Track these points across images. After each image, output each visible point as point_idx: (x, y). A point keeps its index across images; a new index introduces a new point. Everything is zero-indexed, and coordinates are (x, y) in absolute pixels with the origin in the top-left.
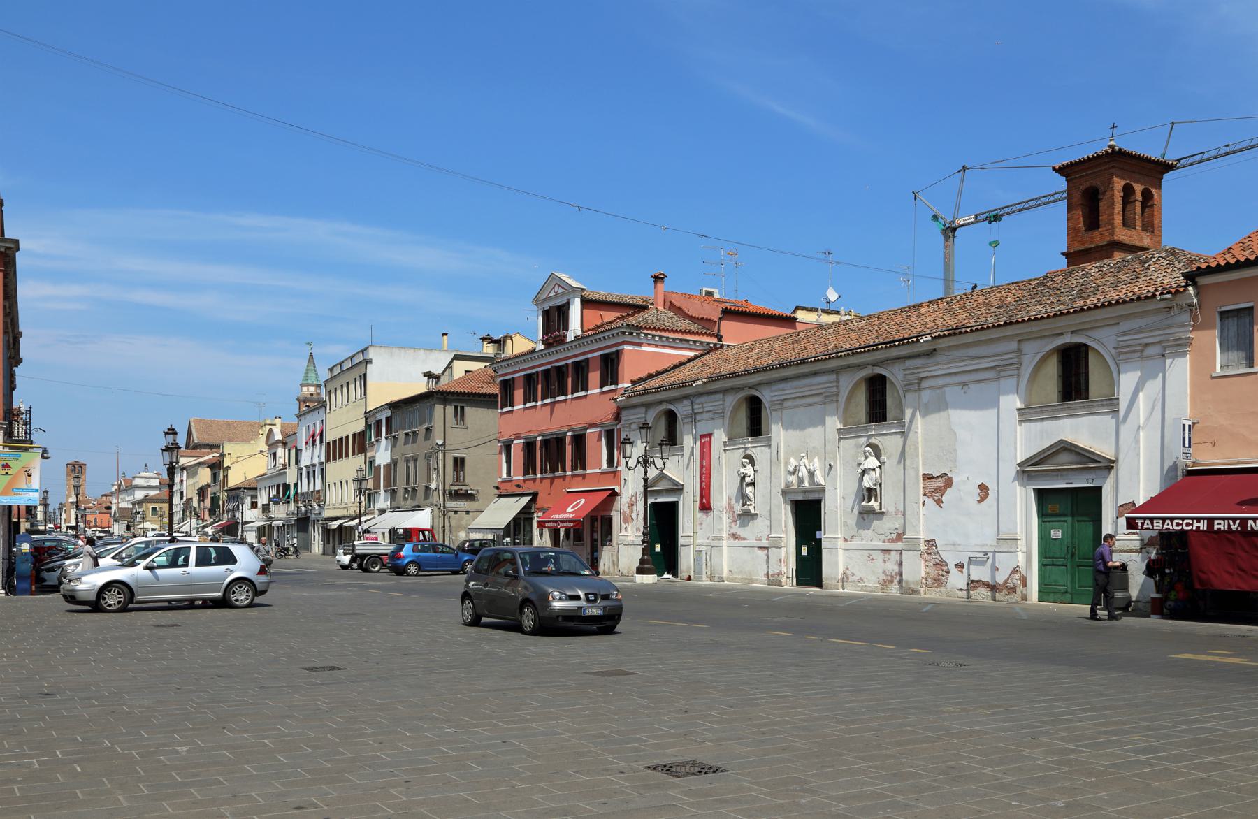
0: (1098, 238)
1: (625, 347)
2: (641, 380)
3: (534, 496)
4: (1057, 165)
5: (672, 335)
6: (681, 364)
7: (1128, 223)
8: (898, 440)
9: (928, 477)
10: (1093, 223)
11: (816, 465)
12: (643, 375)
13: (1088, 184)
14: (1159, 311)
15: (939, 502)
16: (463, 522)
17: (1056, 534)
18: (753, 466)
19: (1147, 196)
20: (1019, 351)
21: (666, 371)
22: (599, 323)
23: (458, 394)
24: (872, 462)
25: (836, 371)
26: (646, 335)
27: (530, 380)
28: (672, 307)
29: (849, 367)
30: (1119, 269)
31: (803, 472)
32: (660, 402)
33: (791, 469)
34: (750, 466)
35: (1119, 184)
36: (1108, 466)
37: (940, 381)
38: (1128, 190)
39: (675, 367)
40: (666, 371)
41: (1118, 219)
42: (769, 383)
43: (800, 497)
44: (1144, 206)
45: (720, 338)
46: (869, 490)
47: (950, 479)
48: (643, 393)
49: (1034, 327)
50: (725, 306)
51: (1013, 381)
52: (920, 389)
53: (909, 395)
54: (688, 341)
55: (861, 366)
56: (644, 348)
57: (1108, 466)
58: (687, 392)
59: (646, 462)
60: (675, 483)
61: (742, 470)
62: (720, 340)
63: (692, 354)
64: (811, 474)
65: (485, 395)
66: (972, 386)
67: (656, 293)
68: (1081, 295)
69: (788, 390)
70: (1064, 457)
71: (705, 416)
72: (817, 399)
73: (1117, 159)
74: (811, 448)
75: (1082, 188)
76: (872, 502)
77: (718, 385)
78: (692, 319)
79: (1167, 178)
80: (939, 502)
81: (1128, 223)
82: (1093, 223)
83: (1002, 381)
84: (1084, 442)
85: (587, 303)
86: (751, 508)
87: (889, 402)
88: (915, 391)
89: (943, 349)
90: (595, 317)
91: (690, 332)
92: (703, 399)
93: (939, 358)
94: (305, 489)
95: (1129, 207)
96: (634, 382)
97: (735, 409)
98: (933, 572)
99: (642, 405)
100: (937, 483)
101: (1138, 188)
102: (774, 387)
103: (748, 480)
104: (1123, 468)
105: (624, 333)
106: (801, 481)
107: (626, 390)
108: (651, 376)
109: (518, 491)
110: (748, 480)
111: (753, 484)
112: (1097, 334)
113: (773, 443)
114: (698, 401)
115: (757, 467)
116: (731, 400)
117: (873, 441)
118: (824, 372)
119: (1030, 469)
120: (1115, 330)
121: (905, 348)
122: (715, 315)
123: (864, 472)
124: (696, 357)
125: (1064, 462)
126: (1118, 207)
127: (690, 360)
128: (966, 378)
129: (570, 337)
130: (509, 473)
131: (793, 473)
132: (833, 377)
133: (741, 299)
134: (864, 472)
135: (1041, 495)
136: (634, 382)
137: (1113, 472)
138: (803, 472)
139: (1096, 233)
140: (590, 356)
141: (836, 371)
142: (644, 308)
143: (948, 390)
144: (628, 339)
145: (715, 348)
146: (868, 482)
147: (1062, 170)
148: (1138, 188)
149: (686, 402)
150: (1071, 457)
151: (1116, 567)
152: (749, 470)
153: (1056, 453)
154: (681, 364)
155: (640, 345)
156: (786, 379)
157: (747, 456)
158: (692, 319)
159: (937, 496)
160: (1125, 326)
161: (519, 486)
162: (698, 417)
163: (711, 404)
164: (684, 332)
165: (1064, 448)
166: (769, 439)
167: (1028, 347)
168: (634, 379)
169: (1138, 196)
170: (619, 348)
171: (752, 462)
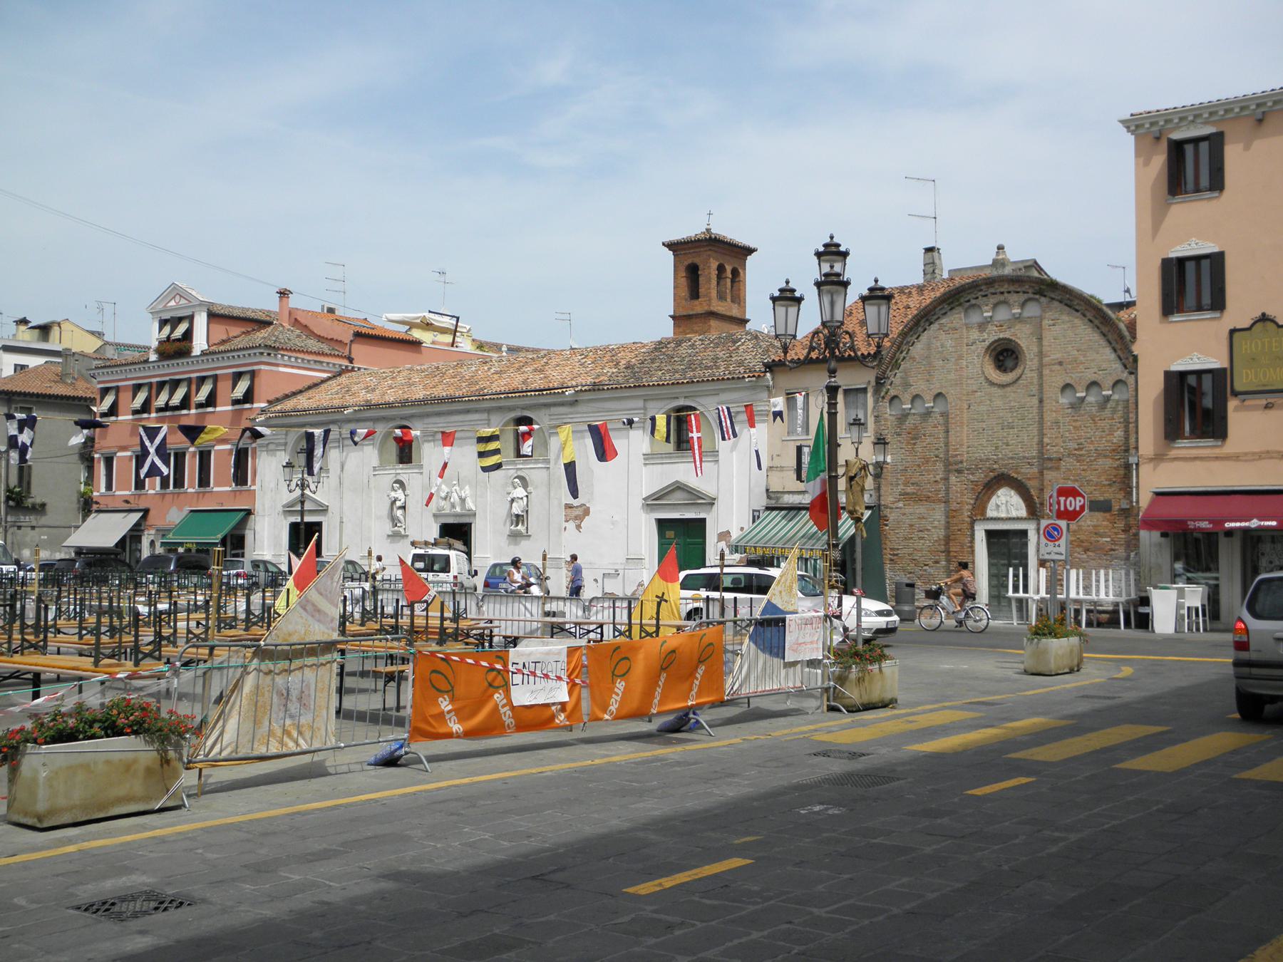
0: (699, 307)
1: (263, 367)
2: (278, 400)
3: (146, 512)
4: (668, 239)
5: (307, 357)
6: (316, 385)
7: (721, 297)
8: (544, 473)
10: (694, 293)
11: (466, 492)
12: (279, 395)
13: (690, 261)
14: (747, 388)
15: (578, 527)
16: (28, 539)
18: (404, 490)
19: (735, 273)
21: (301, 392)
22: (225, 337)
23: (25, 394)
24: (520, 492)
27: (1217, 586)
28: (296, 323)
29: (500, 408)
30: (717, 345)
31: (455, 498)
32: (303, 425)
33: (443, 495)
34: (400, 491)
35: (714, 265)
36: (711, 503)
38: (721, 269)
39: (310, 388)
40: (301, 392)
41: (714, 293)
43: (451, 521)
44: (733, 282)
45: (351, 360)
46: (517, 516)
48: (285, 414)
49: (657, 391)
50: (357, 329)
54: (321, 362)
55: (511, 409)
56: (282, 369)
57: (711, 503)
58: (331, 417)
59: (303, 485)
60: (320, 504)
61: (393, 494)
62: (351, 360)
63: (325, 375)
64: (463, 500)
65: (56, 397)
67: (281, 307)
68: (690, 367)
73: (712, 243)
74: (449, 473)
75: (686, 263)
76: (520, 527)
77: (372, 412)
78: (320, 338)
79: (750, 260)
80: (578, 527)
81: (721, 297)
82: (694, 293)
84: (693, 482)
85: (213, 316)
86: (402, 530)
90: (221, 331)
91: (323, 354)
93: (579, 408)
95: (722, 282)
96: (270, 402)
100: (578, 512)
101: (729, 269)
102: (426, 421)
103: (398, 504)
104: (720, 505)
105: (262, 354)
106: (453, 506)
107: (263, 411)
108: (287, 397)
109: (127, 506)
110: (398, 504)
111: (404, 508)
112: (703, 400)
113: (425, 470)
115: (407, 492)
116: (1226, 364)
117: (520, 473)
118: (476, 411)
119: (655, 500)
122: (347, 337)
123: (513, 500)
124: (329, 379)
125: (678, 498)
126: (714, 282)
127: (324, 381)
129: (196, 351)
130: (109, 486)
131: (445, 499)
134: (513, 500)
135: (661, 523)
136: (270, 402)
137: (715, 507)
138: (455, 498)
139: (696, 302)
142: (270, 323)
144: (265, 359)
145: (347, 370)
146: (517, 509)
147: (671, 246)
148: (729, 269)
150: (684, 495)
151: (1131, 352)
152: (399, 494)
154: (316, 385)
155: (277, 365)
156: (439, 414)
157: (397, 482)
158: (320, 338)
161: (127, 502)
164: (318, 354)
165: (678, 487)
166: (421, 467)
168: (271, 398)
169: (729, 274)
170: (255, 368)
171: (402, 484)
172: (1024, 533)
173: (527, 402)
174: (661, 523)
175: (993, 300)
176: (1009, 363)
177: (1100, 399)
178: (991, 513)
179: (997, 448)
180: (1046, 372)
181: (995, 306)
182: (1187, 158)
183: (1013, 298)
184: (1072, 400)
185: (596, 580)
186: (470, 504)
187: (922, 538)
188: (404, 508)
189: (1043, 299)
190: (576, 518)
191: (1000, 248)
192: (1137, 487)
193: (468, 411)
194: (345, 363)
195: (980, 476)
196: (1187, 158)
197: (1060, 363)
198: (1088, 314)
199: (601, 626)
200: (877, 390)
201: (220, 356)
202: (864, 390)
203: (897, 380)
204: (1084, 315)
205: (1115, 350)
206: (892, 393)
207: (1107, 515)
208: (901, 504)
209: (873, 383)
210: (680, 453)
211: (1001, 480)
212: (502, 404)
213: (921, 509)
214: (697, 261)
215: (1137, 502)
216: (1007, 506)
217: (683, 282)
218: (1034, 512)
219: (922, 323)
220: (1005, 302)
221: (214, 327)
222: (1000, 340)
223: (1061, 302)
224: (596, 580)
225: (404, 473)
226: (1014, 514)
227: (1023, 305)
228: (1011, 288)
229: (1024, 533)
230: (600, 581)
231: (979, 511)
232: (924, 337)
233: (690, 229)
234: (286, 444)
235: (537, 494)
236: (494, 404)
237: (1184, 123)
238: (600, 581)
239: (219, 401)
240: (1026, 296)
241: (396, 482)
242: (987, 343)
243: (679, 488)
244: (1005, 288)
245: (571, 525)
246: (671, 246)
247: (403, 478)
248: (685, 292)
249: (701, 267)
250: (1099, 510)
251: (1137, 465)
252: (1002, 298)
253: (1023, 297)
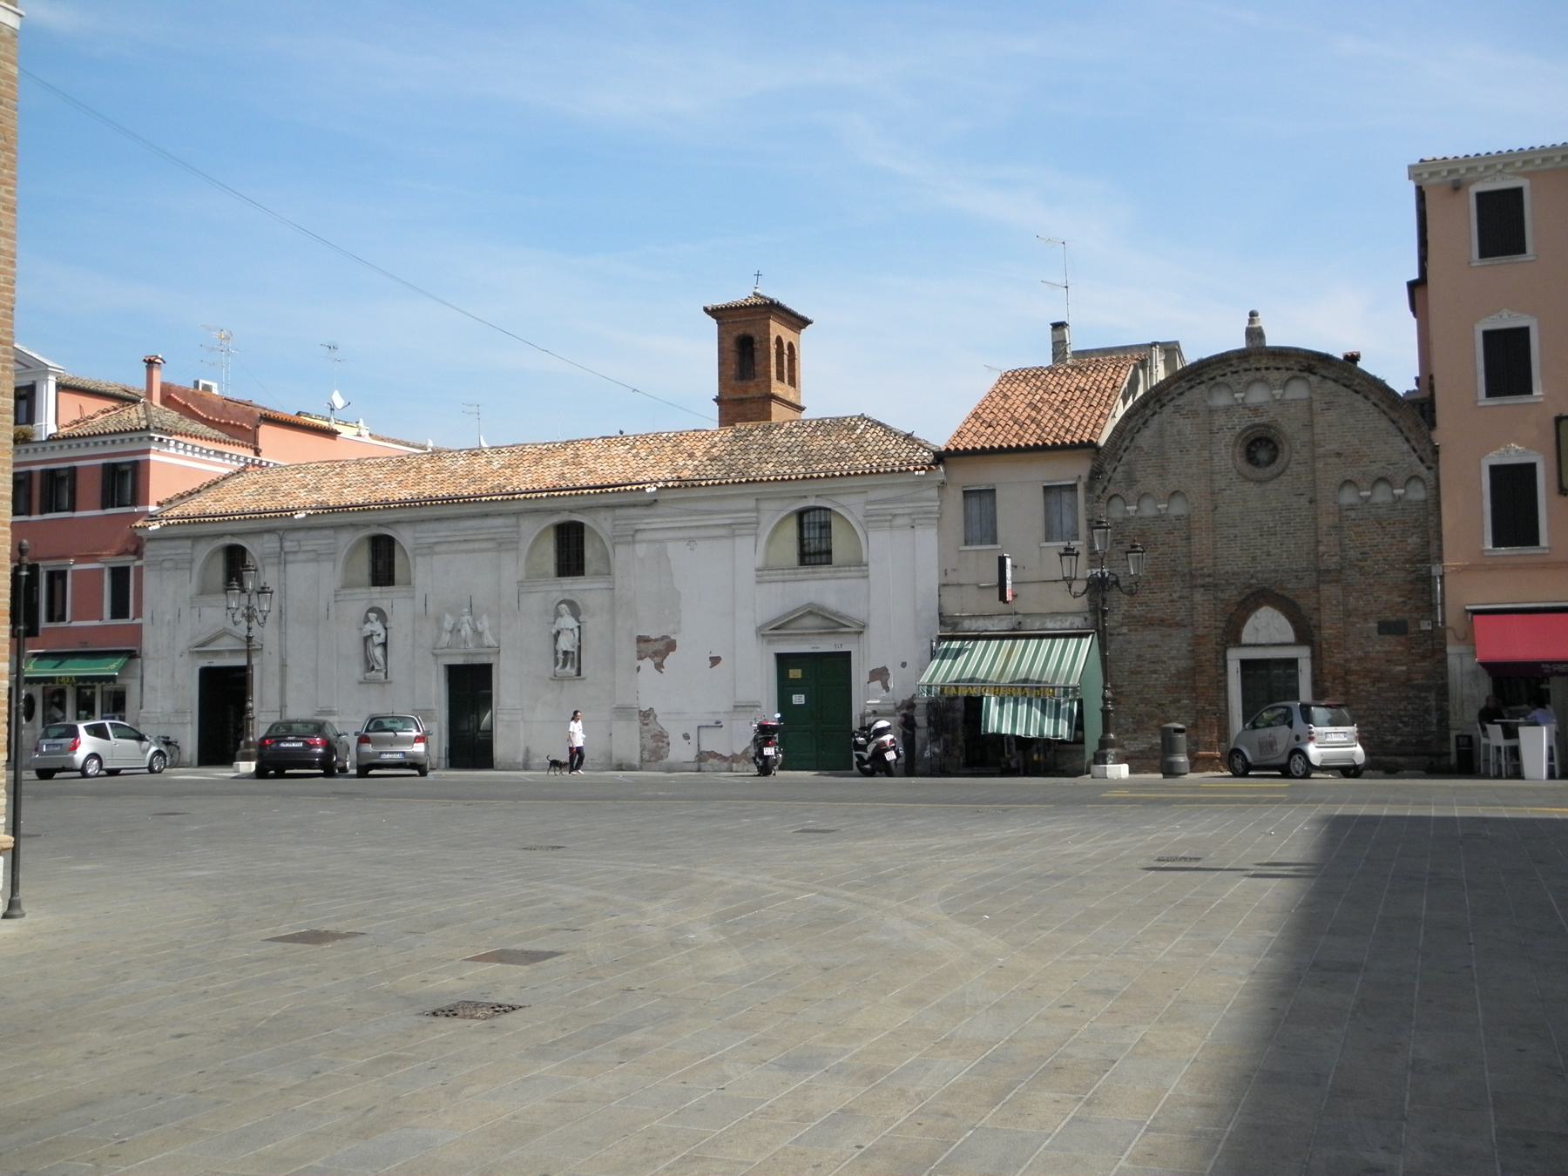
4: (709, 305)
9: (642, 640)
13: (741, 332)
14: (908, 484)
15: (659, 666)
17: (798, 699)
20: (757, 510)
22: (77, 418)
24: (568, 622)
25: (518, 514)
26: (177, 442)
29: (537, 511)
37: (659, 535)
42: (411, 522)
45: (257, 452)
47: (674, 642)
51: (751, 540)
52: (634, 542)
53: (619, 549)
54: (222, 454)
61: (368, 628)
62: (257, 452)
63: (226, 471)
66: (699, 543)
69: (428, 534)
70: (809, 622)
71: (301, 556)
72: (485, 545)
75: (735, 334)
80: (659, 666)
83: (738, 541)
85: (62, 387)
87: (588, 554)
88: (628, 543)
89: (665, 501)
90: (74, 406)
92: (300, 535)
93: (659, 510)
94: (1070, 660)
97: (354, 550)
98: (651, 744)
99: (187, 537)
100: (660, 646)
102: (420, 527)
103: (377, 640)
112: (843, 500)
114: (290, 536)
116: (347, 540)
117: (567, 597)
119: (778, 628)
120: (863, 498)
121: (623, 498)
128: (693, 533)
132: (513, 520)
133: (95, 378)
135: (784, 661)
138: (466, 630)
140: (77, 464)
141: (518, 514)
143: (670, 546)
146: (566, 643)
147: (713, 312)
149: (274, 537)
151: (1431, 442)
153: (801, 617)
156: (439, 519)
159: (658, 659)
160: (873, 495)
162: (290, 558)
163: (313, 542)
165: (813, 611)
167: (765, 505)
170: (139, 458)
171: (382, 616)
172: (1293, 663)
173: (581, 502)
174: (784, 661)
175: (1246, 378)
176: (1263, 455)
177: (1389, 499)
178: (1246, 637)
179: (1254, 559)
180: (1320, 465)
181: (1249, 384)
182: (1484, 212)
183: (1273, 375)
184: (866, 698)
185: (686, 737)
186: (489, 639)
187: (1155, 672)
188: (384, 645)
189: (1312, 378)
190: (655, 654)
191: (1253, 314)
192: (1443, 604)
193: (486, 515)
194: (250, 454)
195: (1232, 594)
196: (1484, 212)
197: (1339, 455)
198: (1372, 397)
199: (1348, 614)
200: (1090, 488)
201: (82, 441)
202: (1073, 488)
203: (1118, 476)
204: (1366, 397)
205: (1408, 440)
206: (1112, 490)
207: (1402, 639)
208: (1125, 630)
209: (1085, 479)
210: (804, 570)
211: (1258, 596)
212: (501, 508)
213: (1152, 636)
214: (751, 331)
215: (1443, 622)
216: (1268, 630)
217: (732, 357)
218: (1304, 634)
219: (1151, 404)
220: (1263, 380)
221: (61, 394)
222: (1255, 426)
223: (1335, 381)
224: (686, 737)
225: (381, 596)
226: (1278, 639)
227: (1285, 385)
228: (1272, 364)
229: (1293, 663)
230: (693, 735)
231: (1232, 637)
232: (1154, 423)
233: (737, 293)
234: (192, 561)
235: (593, 625)
236: (529, 506)
237: (1491, 172)
238: (693, 735)
239: (100, 472)
240: (1290, 373)
241: (372, 610)
242: (1238, 430)
243: (811, 613)
244: (1264, 362)
245: (647, 664)
246: (713, 312)
247: (384, 605)
248: (733, 369)
249: (757, 339)
250: (1389, 633)
251: (1442, 577)
252: (1258, 375)
253: (1286, 375)
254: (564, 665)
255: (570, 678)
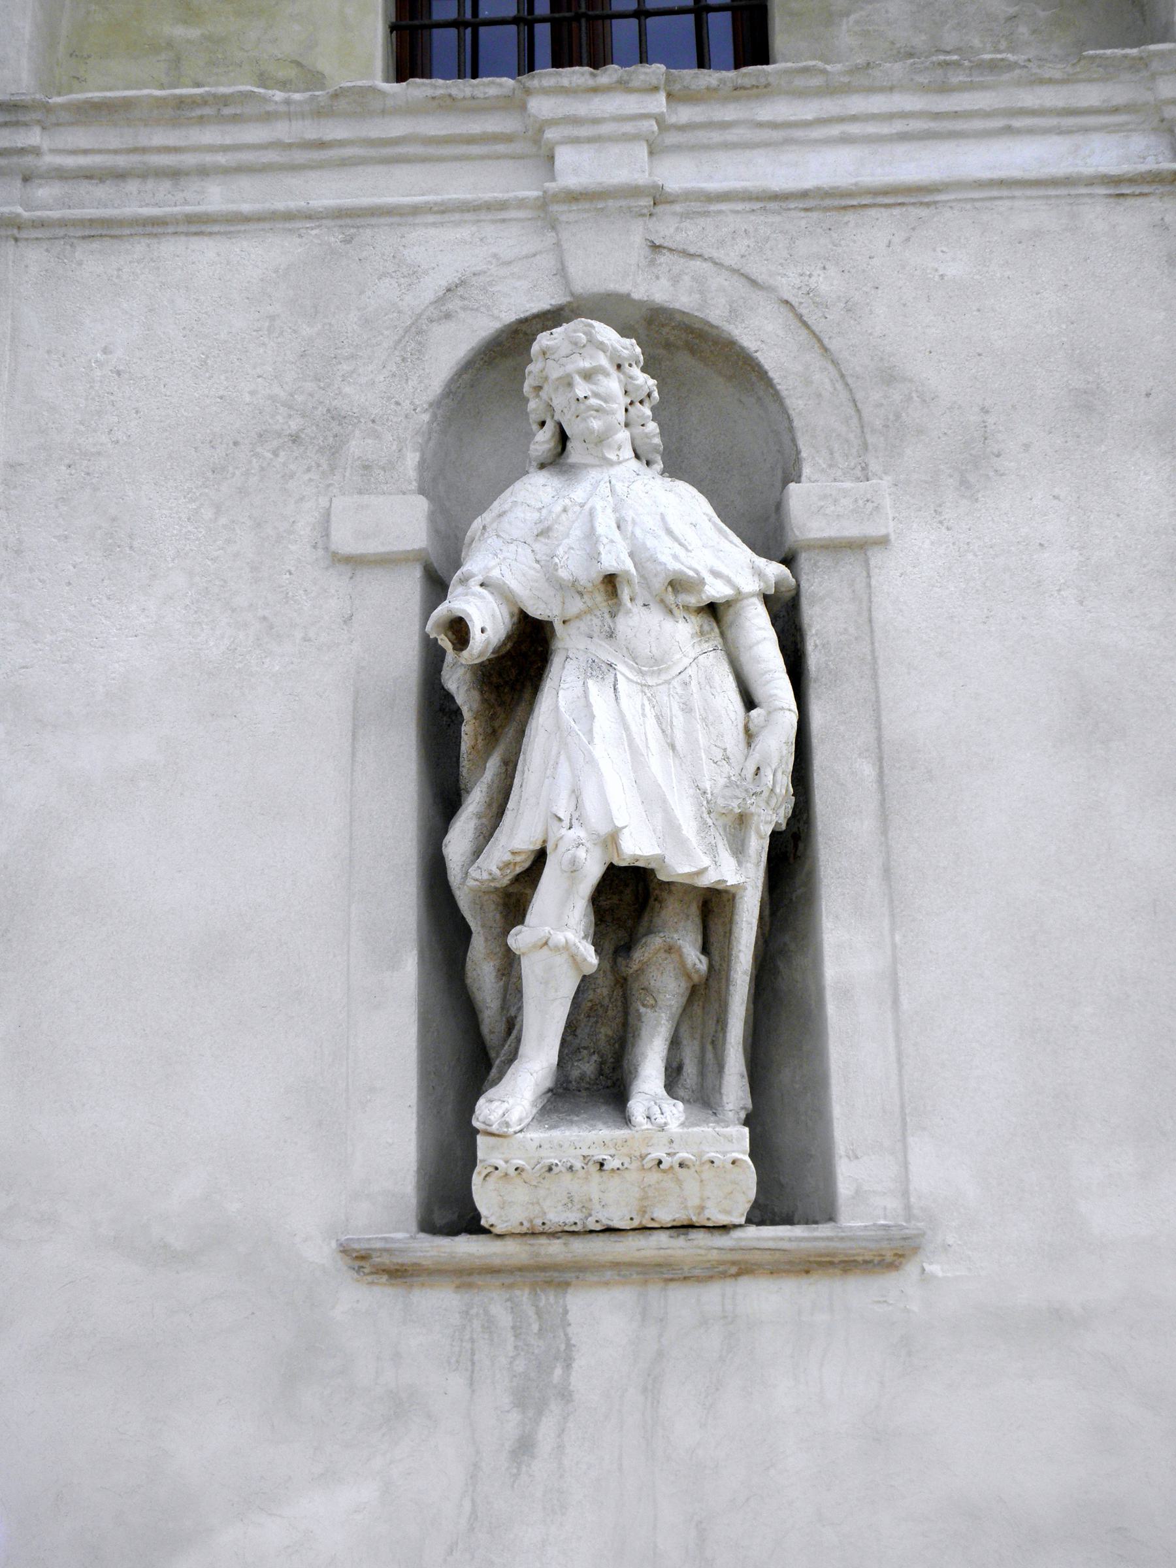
117: (609, 260)
146: (636, 766)
235: (948, 597)
254: (595, 1080)
255: (662, 1252)
